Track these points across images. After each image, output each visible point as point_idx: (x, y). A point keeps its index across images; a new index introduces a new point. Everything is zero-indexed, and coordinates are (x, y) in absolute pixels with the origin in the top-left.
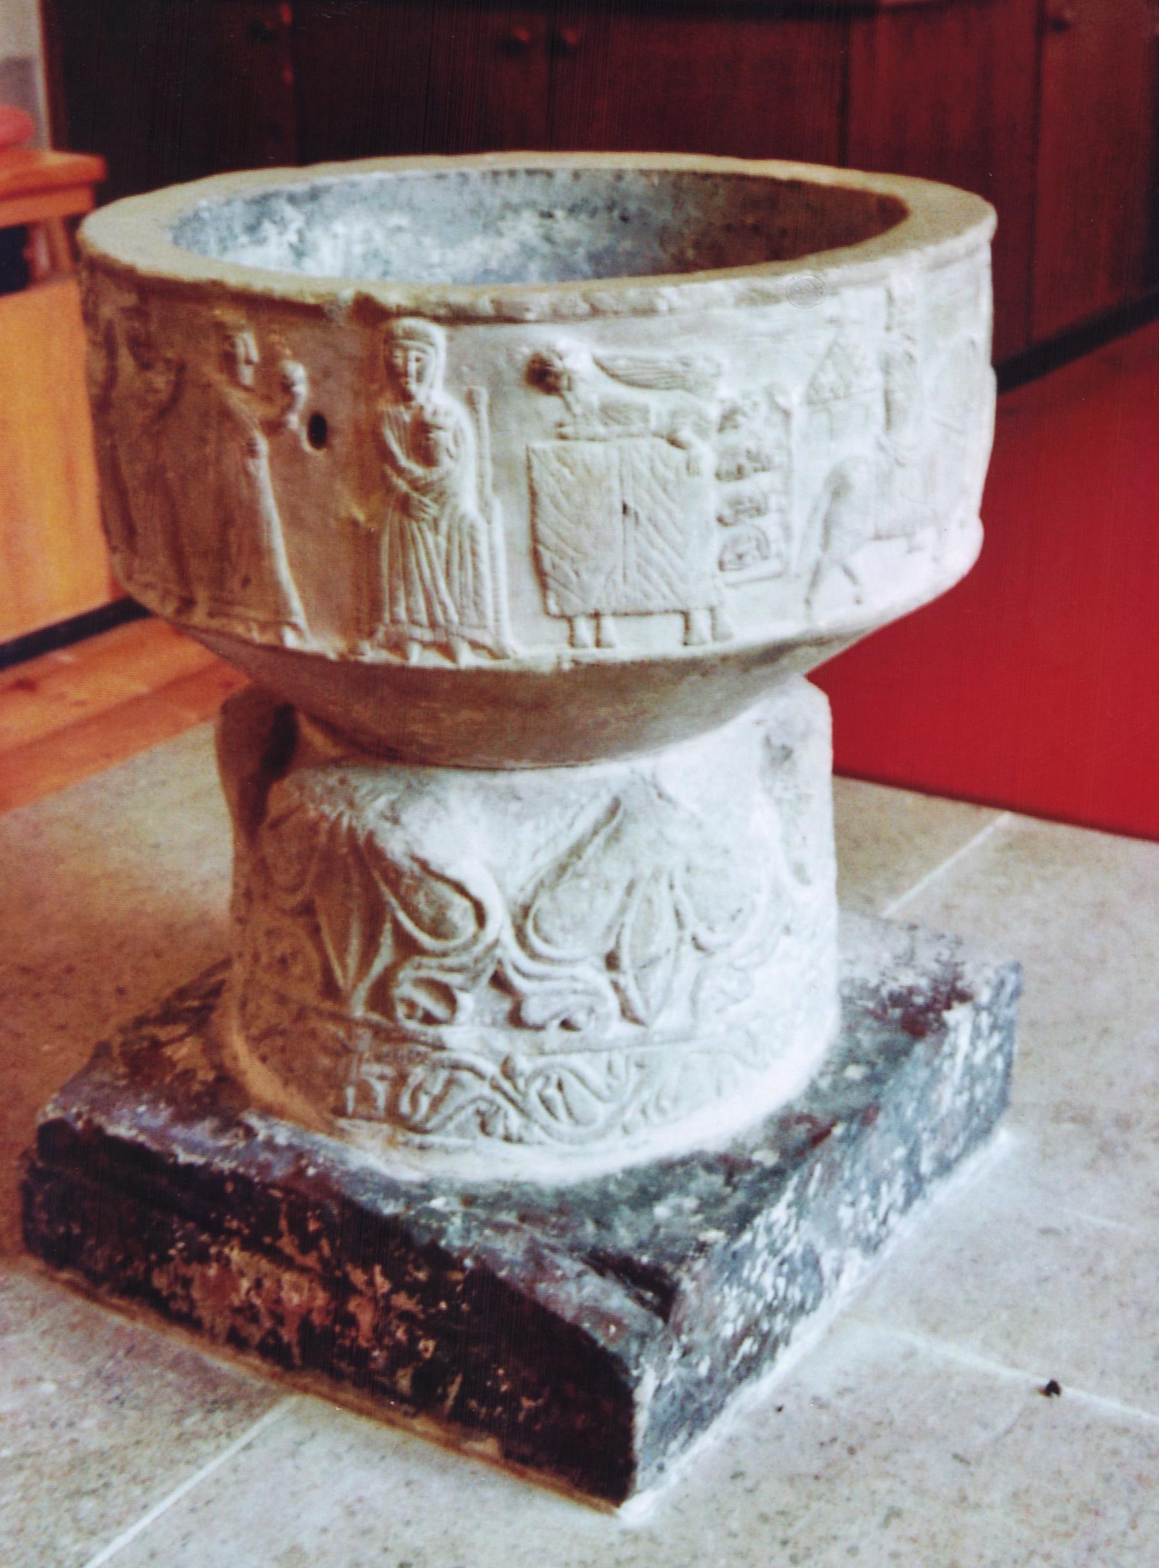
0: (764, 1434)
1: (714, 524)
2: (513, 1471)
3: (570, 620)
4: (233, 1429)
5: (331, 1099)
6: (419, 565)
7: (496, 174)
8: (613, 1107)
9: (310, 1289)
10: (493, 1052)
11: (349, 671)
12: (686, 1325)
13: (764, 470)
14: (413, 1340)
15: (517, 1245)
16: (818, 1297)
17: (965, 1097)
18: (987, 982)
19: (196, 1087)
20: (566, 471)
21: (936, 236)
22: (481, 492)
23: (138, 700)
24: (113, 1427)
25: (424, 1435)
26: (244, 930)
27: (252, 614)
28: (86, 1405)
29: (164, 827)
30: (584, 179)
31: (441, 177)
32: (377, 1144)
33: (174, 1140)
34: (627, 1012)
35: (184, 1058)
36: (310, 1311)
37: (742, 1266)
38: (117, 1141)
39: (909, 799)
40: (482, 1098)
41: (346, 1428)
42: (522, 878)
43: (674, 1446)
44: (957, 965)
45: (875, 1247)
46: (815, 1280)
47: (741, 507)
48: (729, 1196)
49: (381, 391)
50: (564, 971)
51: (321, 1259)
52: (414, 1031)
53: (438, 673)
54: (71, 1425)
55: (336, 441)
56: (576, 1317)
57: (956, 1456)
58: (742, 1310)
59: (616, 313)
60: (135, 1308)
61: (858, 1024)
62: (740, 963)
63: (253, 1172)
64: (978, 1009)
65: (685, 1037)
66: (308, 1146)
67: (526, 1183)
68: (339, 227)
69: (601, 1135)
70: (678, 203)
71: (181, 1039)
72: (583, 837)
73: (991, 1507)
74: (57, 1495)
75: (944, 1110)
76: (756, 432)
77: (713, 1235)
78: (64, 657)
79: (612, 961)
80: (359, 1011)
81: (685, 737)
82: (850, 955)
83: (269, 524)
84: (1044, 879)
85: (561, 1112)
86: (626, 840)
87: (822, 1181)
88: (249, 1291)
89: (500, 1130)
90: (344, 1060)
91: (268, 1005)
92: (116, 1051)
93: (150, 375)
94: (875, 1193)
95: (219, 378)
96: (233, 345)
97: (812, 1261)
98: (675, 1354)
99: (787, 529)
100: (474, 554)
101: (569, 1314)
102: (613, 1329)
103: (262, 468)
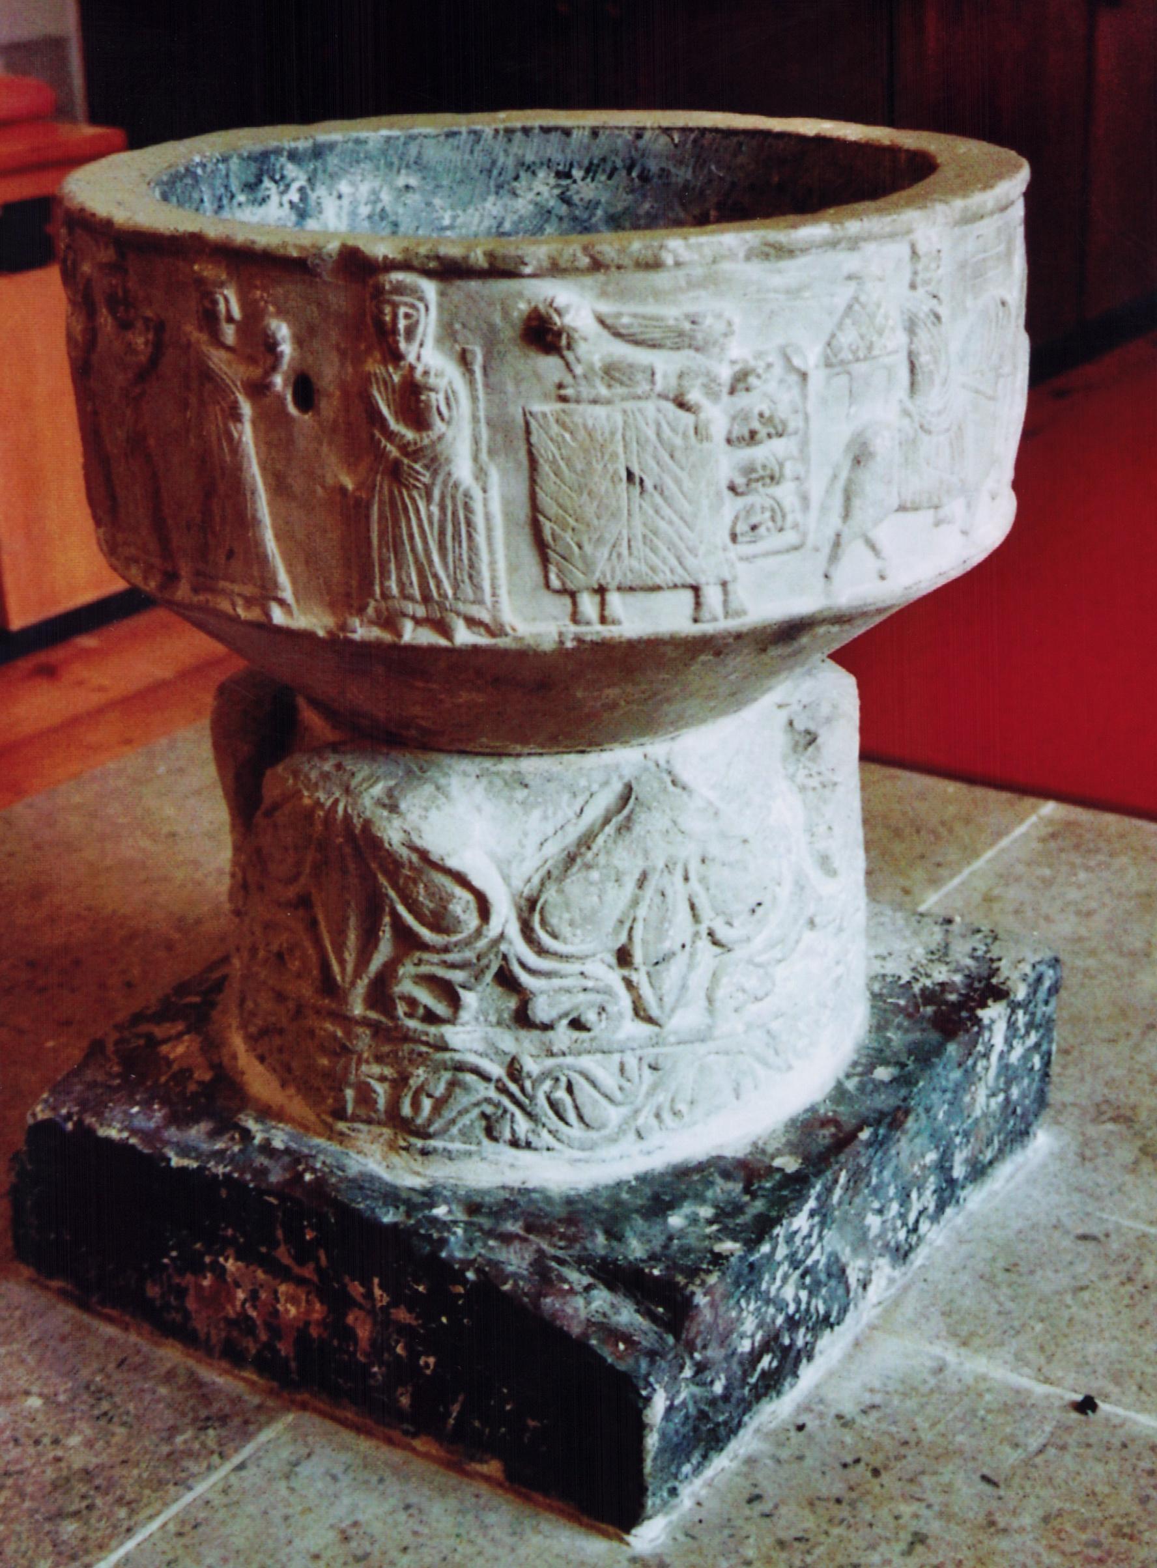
0: (784, 1454)
1: (727, 494)
2: (519, 1494)
3: (573, 595)
4: (225, 1448)
5: (330, 1101)
6: (411, 537)
7: (509, 132)
8: (624, 1110)
9: (308, 1301)
10: (499, 1052)
11: (337, 645)
12: (699, 1342)
13: (780, 435)
14: (414, 1355)
15: (523, 1258)
16: (844, 1310)
17: (1001, 1097)
18: (1024, 978)
19: (192, 1087)
20: (567, 436)
21: (964, 187)
22: (476, 458)
23: (163, 684)
24: (99, 1445)
25: (426, 1456)
26: (242, 921)
27: (236, 588)
28: (73, 1420)
29: (161, 818)
30: (602, 138)
31: (451, 135)
32: (377, 1149)
33: (167, 1143)
34: (640, 1012)
35: (182, 1056)
36: (307, 1324)
37: (760, 1279)
38: (108, 1141)
39: (951, 788)
40: (488, 1100)
41: (344, 1447)
42: (527, 869)
43: (687, 1468)
44: (992, 960)
45: (906, 1255)
46: (841, 1291)
47: (754, 476)
48: (746, 1204)
49: (369, 351)
50: (575, 967)
51: (319, 1270)
52: (415, 1031)
53: (432, 650)
54: (56, 1442)
55: (323, 404)
56: (585, 1335)
57: (985, 1479)
58: (760, 1326)
59: (619, 267)
60: (127, 1318)
61: (887, 1021)
62: (758, 959)
63: (248, 1177)
64: (1014, 1006)
65: (703, 1037)
66: (306, 1151)
67: (534, 1190)
68: (344, 187)
69: (613, 1140)
70: (700, 161)
71: (179, 1036)
72: (593, 825)
73: (1022, 1530)
74: (38, 1516)
75: (977, 1113)
76: (771, 394)
77: (728, 1246)
78: (88, 642)
79: (624, 957)
80: (358, 1009)
81: (703, 721)
82: (882, 950)
83: (253, 492)
84: (1088, 869)
85: (571, 1116)
86: (638, 829)
87: (846, 1189)
88: (245, 1301)
89: (507, 1135)
90: (343, 1061)
91: (266, 1003)
92: (110, 1047)
93: (129, 336)
94: (905, 1198)
95: (199, 337)
96: (215, 303)
97: (838, 1272)
98: (688, 1373)
99: (805, 499)
100: (469, 523)
101: (576, 1330)
102: (622, 1346)
103: (247, 434)
